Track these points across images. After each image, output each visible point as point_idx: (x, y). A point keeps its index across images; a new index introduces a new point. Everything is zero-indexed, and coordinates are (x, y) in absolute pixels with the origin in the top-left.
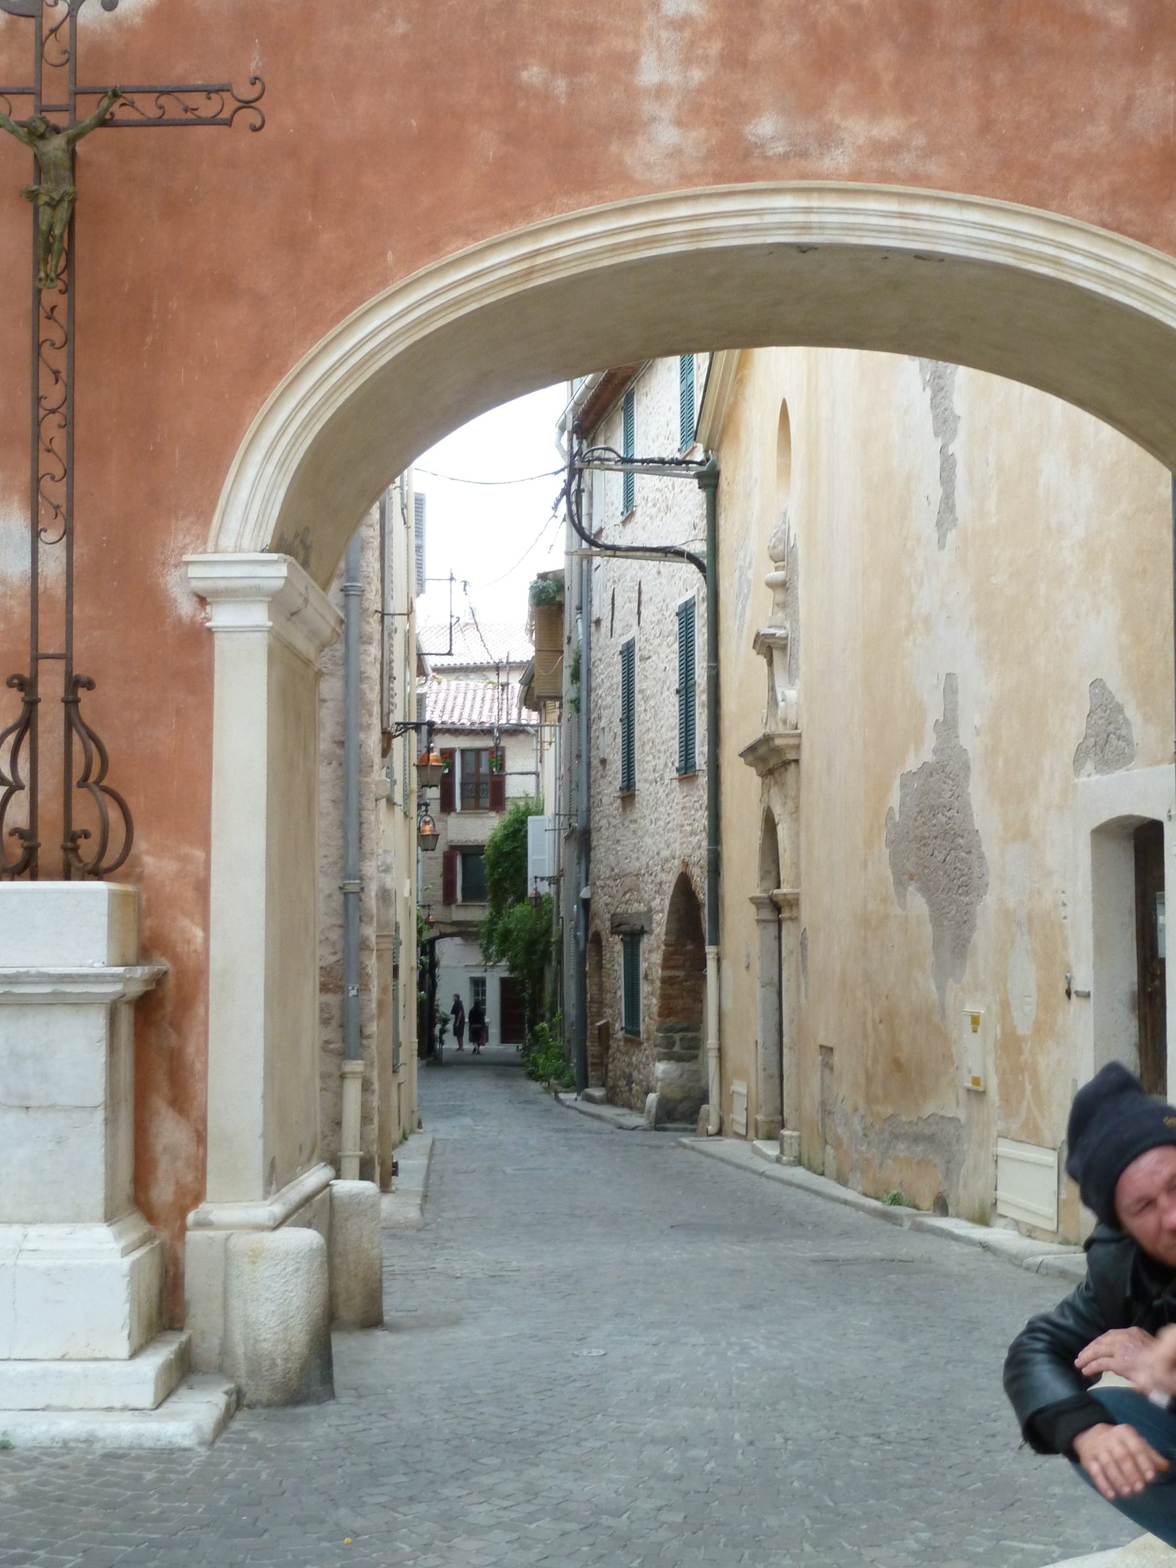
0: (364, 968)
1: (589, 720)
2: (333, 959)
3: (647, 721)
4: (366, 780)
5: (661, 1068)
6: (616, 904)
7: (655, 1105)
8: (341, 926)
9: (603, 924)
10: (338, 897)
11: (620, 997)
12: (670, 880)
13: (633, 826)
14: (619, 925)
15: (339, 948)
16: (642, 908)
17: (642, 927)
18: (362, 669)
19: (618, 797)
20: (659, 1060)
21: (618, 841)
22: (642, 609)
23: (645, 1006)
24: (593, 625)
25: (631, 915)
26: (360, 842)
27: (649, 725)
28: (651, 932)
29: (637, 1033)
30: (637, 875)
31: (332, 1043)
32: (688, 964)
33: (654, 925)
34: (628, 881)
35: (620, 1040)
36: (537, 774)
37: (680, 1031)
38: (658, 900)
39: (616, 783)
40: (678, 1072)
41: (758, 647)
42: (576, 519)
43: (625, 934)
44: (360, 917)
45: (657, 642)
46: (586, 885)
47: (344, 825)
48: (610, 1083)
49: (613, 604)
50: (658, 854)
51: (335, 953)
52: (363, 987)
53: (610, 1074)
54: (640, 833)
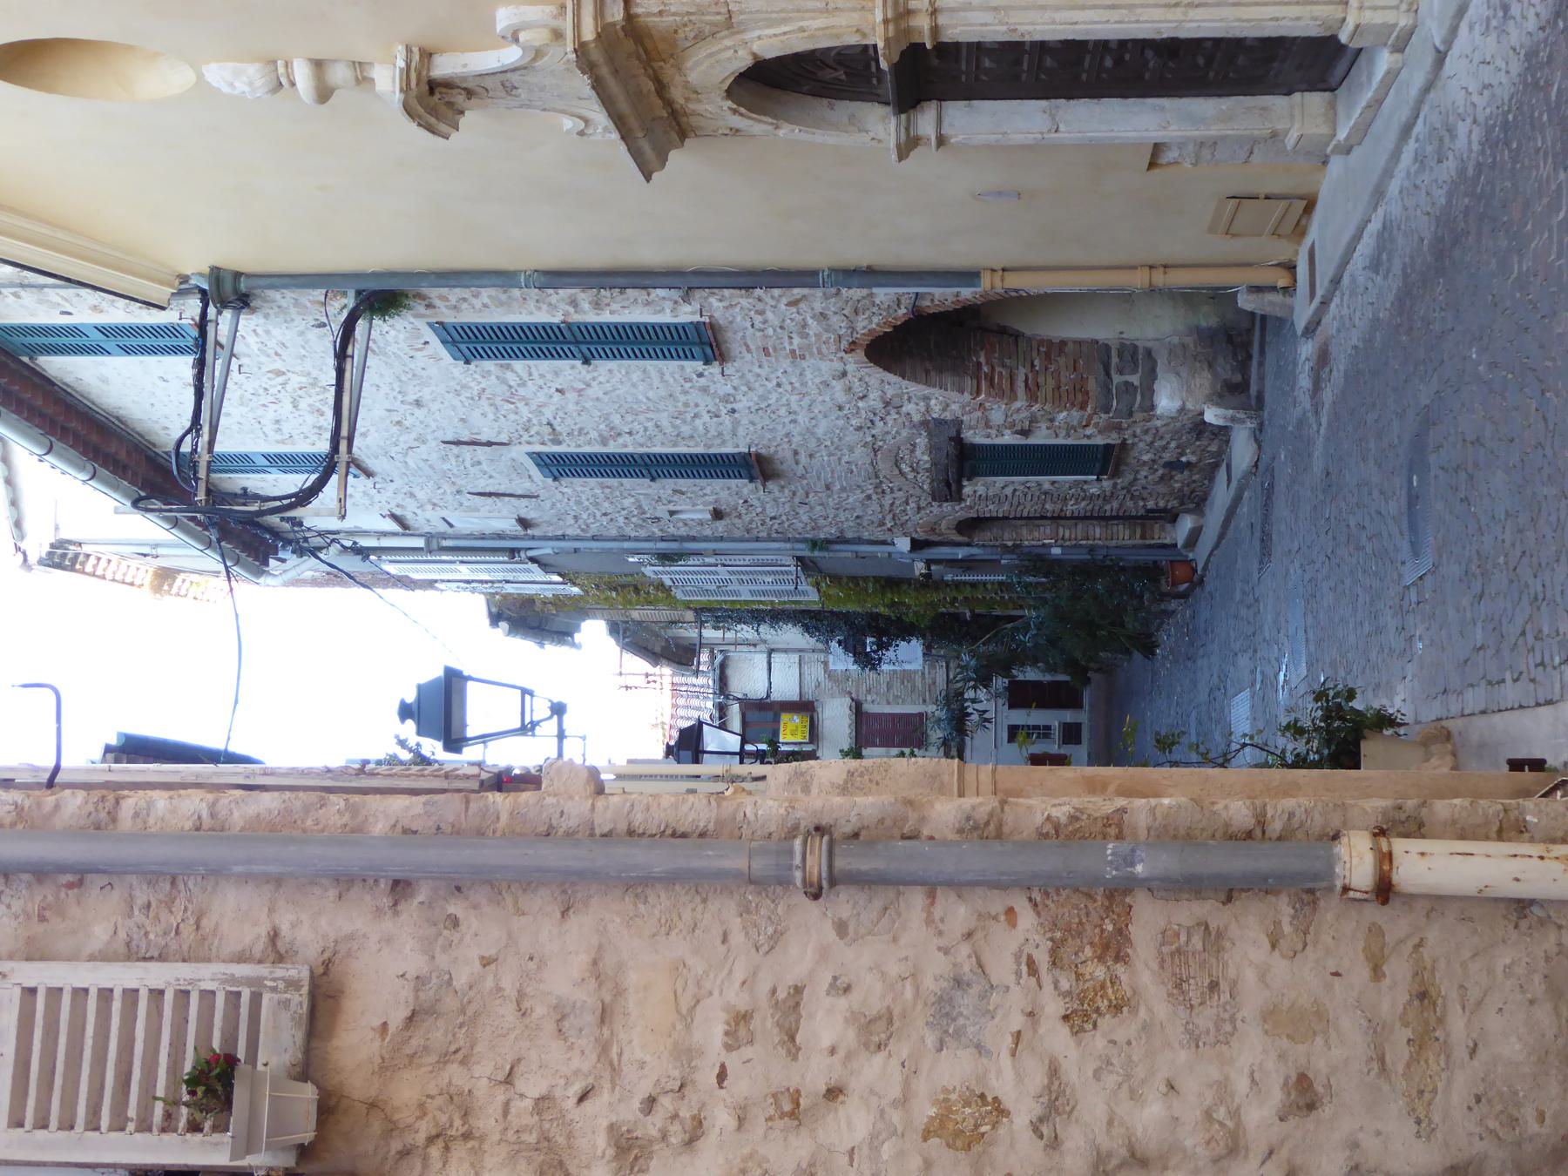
0: (1057, 827)
1: (662, 539)
2: (1027, 919)
3: (646, 429)
4: (504, 817)
5: (1167, 401)
6: (918, 492)
7: (1220, 411)
8: (932, 896)
9: (951, 512)
10: (843, 903)
11: (1053, 483)
12: (881, 383)
13: (803, 458)
14: (948, 485)
15: (996, 903)
16: (922, 441)
17: (951, 439)
18: (188, 825)
19: (764, 486)
20: (1152, 407)
21: (828, 487)
22: (483, 438)
23: (1068, 435)
24: (529, 532)
25: (934, 464)
26: (684, 835)
27: (650, 425)
28: (958, 423)
29: (1108, 448)
30: (875, 451)
31: (1277, 924)
32: (1007, 361)
33: (947, 415)
34: (885, 468)
35: (1115, 485)
36: (771, 652)
37: (1108, 374)
38: (909, 407)
39: (745, 491)
40: (1173, 378)
41: (443, 127)
42: (285, 502)
43: (960, 476)
44: (904, 837)
45: (525, 411)
46: (893, 544)
47: (637, 884)
48: (1174, 503)
49: (490, 495)
50: (840, 408)
51: (1010, 912)
52: (1112, 831)
53: (1162, 504)
54: (812, 444)
